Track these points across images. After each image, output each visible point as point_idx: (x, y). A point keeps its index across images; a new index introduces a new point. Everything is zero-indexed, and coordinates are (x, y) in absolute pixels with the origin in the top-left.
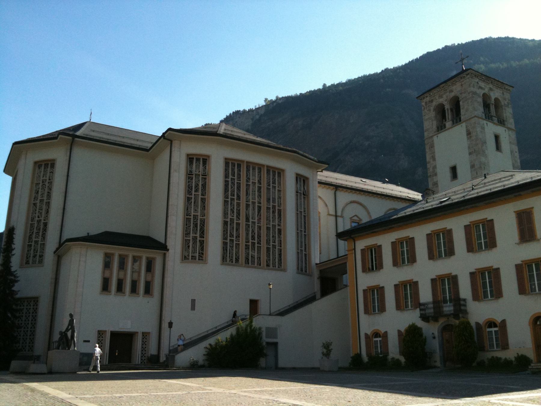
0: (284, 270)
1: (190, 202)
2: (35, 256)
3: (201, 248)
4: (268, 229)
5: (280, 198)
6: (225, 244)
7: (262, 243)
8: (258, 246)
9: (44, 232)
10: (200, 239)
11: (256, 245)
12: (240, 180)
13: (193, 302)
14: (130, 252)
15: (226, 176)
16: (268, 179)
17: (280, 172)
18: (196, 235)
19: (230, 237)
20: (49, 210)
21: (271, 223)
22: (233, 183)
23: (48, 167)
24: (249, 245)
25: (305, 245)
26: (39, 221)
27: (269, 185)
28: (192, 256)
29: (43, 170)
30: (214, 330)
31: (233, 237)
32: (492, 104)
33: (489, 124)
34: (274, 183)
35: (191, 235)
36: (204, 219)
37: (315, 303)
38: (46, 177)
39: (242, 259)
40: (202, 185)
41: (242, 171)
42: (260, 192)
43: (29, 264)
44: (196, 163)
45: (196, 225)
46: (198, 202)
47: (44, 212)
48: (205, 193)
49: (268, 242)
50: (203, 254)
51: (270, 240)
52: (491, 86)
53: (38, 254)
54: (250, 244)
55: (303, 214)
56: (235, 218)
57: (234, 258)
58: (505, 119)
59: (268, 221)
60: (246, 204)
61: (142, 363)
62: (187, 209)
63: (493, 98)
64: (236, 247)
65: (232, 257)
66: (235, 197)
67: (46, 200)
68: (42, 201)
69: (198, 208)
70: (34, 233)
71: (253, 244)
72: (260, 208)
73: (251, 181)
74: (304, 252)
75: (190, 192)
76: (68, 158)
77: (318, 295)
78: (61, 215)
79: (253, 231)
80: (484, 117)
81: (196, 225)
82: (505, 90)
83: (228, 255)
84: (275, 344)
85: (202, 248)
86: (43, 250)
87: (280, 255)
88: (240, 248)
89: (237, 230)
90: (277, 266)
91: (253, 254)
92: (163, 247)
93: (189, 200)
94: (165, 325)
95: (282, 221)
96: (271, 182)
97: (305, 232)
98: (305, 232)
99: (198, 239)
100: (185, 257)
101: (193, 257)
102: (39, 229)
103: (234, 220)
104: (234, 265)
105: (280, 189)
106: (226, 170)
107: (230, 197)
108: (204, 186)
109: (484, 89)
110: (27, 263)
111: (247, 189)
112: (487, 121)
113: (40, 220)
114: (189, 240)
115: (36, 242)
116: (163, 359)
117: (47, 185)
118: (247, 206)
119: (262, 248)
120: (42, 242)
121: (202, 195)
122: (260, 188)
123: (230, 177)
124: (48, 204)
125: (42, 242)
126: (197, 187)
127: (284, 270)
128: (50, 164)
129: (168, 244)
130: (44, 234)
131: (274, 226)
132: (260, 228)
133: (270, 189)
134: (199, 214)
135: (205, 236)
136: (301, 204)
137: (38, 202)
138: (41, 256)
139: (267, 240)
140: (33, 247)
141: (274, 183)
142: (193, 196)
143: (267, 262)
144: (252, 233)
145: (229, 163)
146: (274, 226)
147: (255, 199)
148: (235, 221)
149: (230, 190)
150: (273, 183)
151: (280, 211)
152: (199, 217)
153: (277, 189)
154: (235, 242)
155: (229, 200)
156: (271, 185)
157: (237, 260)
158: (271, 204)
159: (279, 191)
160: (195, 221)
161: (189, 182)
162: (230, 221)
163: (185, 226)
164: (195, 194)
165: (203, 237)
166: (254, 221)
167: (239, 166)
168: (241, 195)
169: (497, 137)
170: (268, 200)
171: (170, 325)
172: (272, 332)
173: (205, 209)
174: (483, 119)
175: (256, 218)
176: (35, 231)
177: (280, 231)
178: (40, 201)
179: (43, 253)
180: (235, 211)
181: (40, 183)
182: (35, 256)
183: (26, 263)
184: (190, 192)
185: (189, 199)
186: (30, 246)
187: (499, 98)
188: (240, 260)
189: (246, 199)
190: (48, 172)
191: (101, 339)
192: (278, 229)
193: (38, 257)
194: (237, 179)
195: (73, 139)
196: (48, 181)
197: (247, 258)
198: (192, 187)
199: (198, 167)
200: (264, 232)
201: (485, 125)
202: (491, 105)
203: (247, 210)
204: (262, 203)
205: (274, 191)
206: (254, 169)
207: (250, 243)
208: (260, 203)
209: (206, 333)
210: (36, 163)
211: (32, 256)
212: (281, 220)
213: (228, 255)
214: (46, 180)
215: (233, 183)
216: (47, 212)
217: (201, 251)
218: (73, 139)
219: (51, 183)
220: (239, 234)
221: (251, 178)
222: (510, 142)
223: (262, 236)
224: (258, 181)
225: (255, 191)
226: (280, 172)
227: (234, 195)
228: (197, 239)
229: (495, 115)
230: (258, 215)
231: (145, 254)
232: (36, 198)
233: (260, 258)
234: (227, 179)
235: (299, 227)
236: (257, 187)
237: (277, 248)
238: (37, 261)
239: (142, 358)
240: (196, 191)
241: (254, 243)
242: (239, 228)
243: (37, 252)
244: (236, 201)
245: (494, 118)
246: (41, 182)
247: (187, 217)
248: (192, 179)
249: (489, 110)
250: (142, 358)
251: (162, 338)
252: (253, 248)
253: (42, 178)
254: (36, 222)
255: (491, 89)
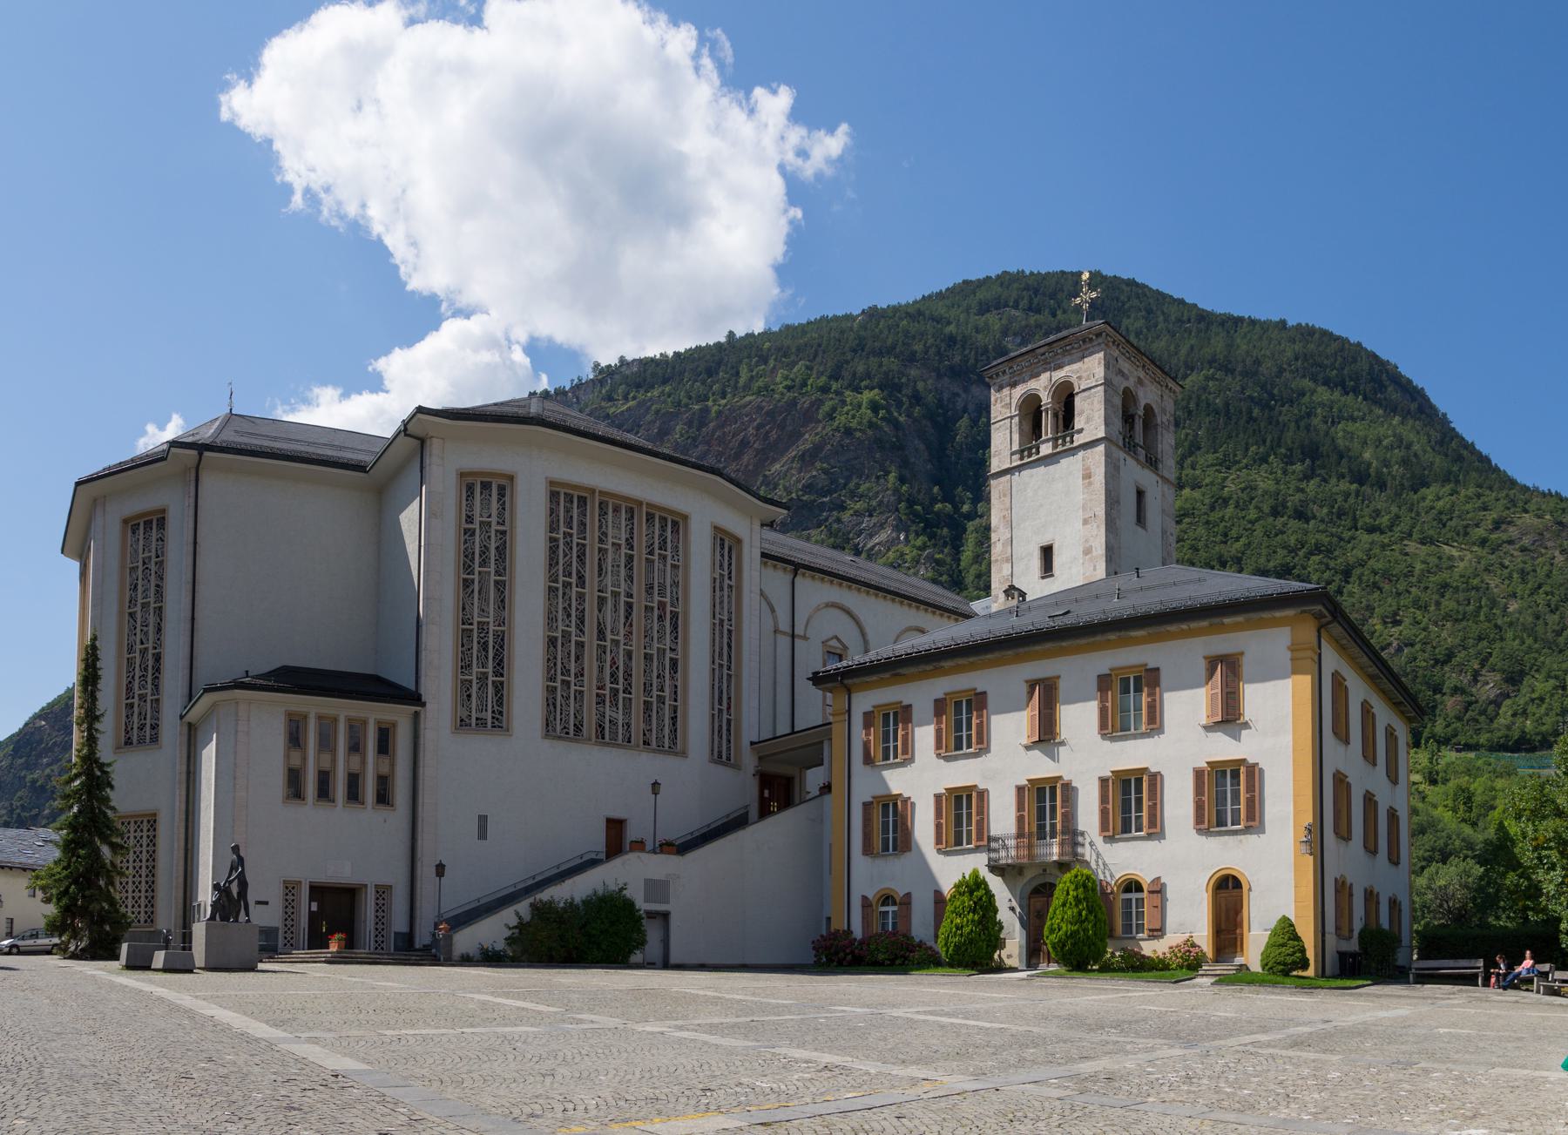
0: (683, 754)
1: (470, 590)
2: (141, 728)
3: (497, 701)
4: (648, 657)
5: (675, 584)
6: (551, 691)
7: (633, 691)
8: (624, 698)
9: (157, 674)
10: (495, 679)
11: (621, 695)
12: (585, 539)
13: (483, 820)
14: (344, 709)
15: (553, 527)
16: (651, 536)
17: (675, 523)
18: (484, 670)
19: (562, 674)
20: (163, 625)
21: (656, 645)
22: (568, 545)
23: (151, 529)
24: (604, 695)
25: (729, 698)
26: (144, 652)
27: (651, 553)
28: (477, 719)
29: (141, 537)
30: (531, 882)
31: (569, 676)
32: (1140, 416)
33: (1129, 459)
34: (663, 546)
35: (475, 669)
36: (503, 632)
37: (750, 830)
38: (150, 552)
39: (589, 727)
40: (497, 548)
41: (588, 514)
42: (631, 569)
43: (131, 743)
44: (481, 493)
45: (484, 647)
46: (488, 592)
47: (151, 629)
48: (505, 569)
49: (647, 689)
50: (501, 713)
51: (651, 685)
52: (1142, 374)
53: (148, 722)
54: (607, 692)
55: (726, 627)
56: (573, 629)
57: (572, 723)
58: (1159, 457)
59: (647, 639)
60: (599, 597)
61: (376, 948)
62: (464, 609)
63: (1142, 403)
64: (575, 699)
65: (567, 722)
66: (574, 580)
67: (155, 602)
68: (145, 606)
69: (488, 604)
70: (137, 677)
71: (615, 692)
72: (629, 606)
73: (610, 540)
74: (725, 716)
75: (470, 566)
76: (192, 500)
77: (754, 812)
78: (188, 633)
79: (613, 662)
80: (1121, 444)
81: (484, 647)
82: (1167, 391)
83: (558, 717)
84: (665, 916)
85: (500, 702)
86: (158, 712)
87: (674, 719)
88: (585, 702)
89: (577, 658)
90: (667, 745)
91: (614, 715)
92: (413, 698)
93: (468, 587)
94: (426, 871)
95: (679, 641)
96: (656, 546)
97: (729, 669)
98: (729, 669)
99: (491, 678)
100: (462, 720)
101: (479, 722)
102: (146, 670)
103: (570, 635)
104: (571, 740)
105: (676, 563)
106: (552, 512)
107: (561, 579)
108: (501, 550)
109: (1127, 379)
110: (128, 742)
111: (600, 559)
112: (1125, 452)
113: (146, 649)
114: (471, 681)
115: (142, 698)
116: (422, 938)
117: (153, 568)
118: (602, 601)
119: (633, 701)
120: (153, 697)
121: (498, 573)
122: (630, 558)
123: (563, 529)
124: (159, 611)
125: (153, 697)
126: (484, 553)
127: (683, 754)
128: (155, 521)
129: (422, 691)
130: (157, 678)
131: (661, 652)
132: (629, 655)
133: (653, 561)
134: (491, 620)
135: (505, 673)
136: (721, 602)
137: (138, 608)
138: (154, 727)
139: (645, 684)
140: (136, 709)
141: (663, 546)
142: (476, 577)
143: (644, 735)
144: (611, 667)
145: (558, 493)
146: (661, 652)
147: (619, 586)
148: (574, 638)
149: (561, 562)
150: (660, 549)
151: (675, 616)
152: (492, 628)
153: (669, 561)
154: (573, 688)
155: (560, 585)
156: (657, 551)
157: (578, 729)
158: (656, 598)
159: (675, 567)
160: (482, 635)
161: (465, 542)
162: (563, 636)
163: (460, 649)
164: (480, 573)
165: (502, 675)
166: (616, 638)
167: (582, 501)
168: (587, 576)
169: (1140, 494)
170: (650, 588)
171: (440, 870)
172: (657, 888)
173: (504, 608)
174: (1118, 446)
175: (622, 632)
176: (138, 673)
177: (674, 663)
178: (143, 608)
179: (158, 719)
180: (573, 613)
181: (137, 567)
182: (141, 728)
183: (126, 743)
184: (470, 566)
185: (467, 584)
186: (131, 706)
187: (1154, 407)
188: (585, 729)
189: (599, 586)
190: (154, 539)
191: (290, 897)
192: (671, 659)
193: (148, 727)
194: (578, 534)
195: (201, 455)
196: (154, 560)
197: (600, 726)
198: (473, 553)
199: (486, 504)
200: (638, 665)
201: (1122, 461)
202: (1137, 417)
203: (600, 611)
204: (635, 596)
205: (661, 566)
206: (616, 510)
207: (608, 689)
208: (631, 596)
209: (512, 890)
210: (125, 521)
211: (135, 726)
212: (676, 638)
213: (558, 717)
214: (150, 558)
215: (568, 545)
216: (159, 630)
217: (496, 708)
218: (201, 455)
219: (160, 564)
220: (583, 669)
221: (610, 532)
222: (1163, 511)
223: (634, 673)
224: (627, 540)
225: (618, 566)
226: (675, 523)
227: (570, 575)
228: (487, 678)
229: (1142, 444)
230: (625, 624)
231: (375, 713)
232: (133, 602)
233: (628, 725)
234: (554, 535)
235: (717, 657)
236: (623, 555)
237: (667, 703)
238: (148, 738)
239: (377, 939)
240: (484, 563)
241: (617, 690)
242: (583, 655)
243: (145, 719)
244: (575, 589)
245: (1140, 449)
246: (140, 564)
247: (464, 627)
248: (473, 534)
249: (1132, 428)
250: (377, 939)
251: (418, 897)
252: (615, 704)
253: (141, 556)
254: (137, 655)
255: (1140, 382)
